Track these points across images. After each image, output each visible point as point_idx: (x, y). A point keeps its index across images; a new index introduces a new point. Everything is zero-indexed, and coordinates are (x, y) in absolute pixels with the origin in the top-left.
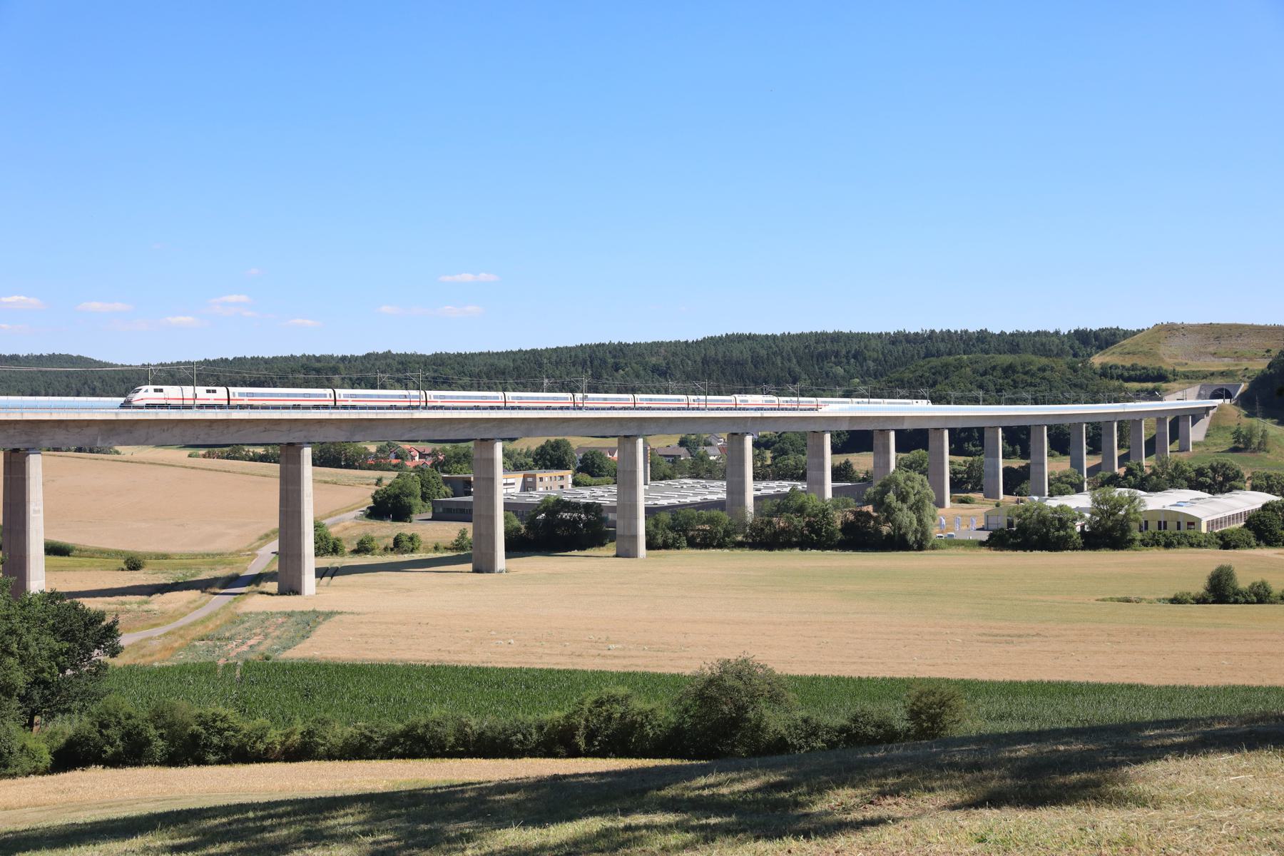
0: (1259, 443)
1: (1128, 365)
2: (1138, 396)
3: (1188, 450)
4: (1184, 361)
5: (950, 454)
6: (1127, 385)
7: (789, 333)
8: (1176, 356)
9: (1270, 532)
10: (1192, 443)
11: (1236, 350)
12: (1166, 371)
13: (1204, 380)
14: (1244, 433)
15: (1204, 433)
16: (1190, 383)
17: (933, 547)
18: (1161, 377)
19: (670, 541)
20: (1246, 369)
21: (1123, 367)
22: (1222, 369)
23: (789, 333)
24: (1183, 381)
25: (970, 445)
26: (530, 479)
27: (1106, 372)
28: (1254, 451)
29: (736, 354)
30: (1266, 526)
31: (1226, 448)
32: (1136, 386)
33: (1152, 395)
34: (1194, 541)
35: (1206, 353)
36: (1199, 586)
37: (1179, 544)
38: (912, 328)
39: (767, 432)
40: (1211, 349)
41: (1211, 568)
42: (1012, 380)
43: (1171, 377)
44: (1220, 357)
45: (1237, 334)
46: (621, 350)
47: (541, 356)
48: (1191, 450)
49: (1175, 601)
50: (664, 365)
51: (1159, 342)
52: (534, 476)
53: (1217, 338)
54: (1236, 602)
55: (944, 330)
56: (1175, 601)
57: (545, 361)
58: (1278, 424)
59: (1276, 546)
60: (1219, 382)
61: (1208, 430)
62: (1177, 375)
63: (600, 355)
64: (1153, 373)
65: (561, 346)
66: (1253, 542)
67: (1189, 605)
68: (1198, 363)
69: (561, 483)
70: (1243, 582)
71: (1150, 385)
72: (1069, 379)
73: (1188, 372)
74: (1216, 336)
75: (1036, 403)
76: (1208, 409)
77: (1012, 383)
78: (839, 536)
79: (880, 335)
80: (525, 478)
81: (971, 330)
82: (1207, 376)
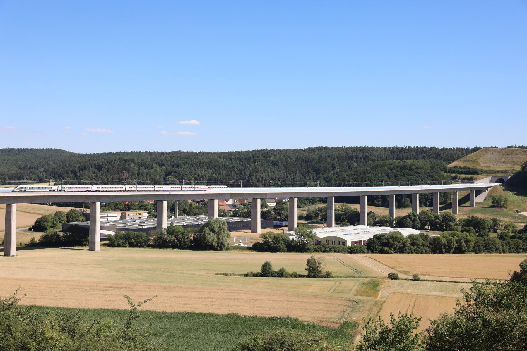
0: (504, 204)
1: (462, 166)
2: (464, 180)
3: (473, 206)
4: (489, 165)
5: (367, 205)
6: (459, 175)
7: (345, 147)
8: (486, 163)
9: (373, 247)
10: (476, 203)
11: (513, 161)
12: (478, 170)
13: (494, 174)
14: (497, 199)
15: (484, 198)
16: (487, 175)
17: (227, 249)
18: (475, 172)
19: (121, 244)
20: (513, 170)
21: (460, 167)
22: (502, 169)
23: (345, 147)
24: (485, 174)
25: (377, 201)
26: (124, 215)
27: (455, 170)
28: (501, 207)
29: (311, 156)
30: (372, 244)
31: (490, 205)
32: (463, 176)
33: (471, 181)
34: (337, 250)
35: (500, 162)
36: (259, 270)
37: (330, 251)
38: (401, 145)
39: (108, 201)
40: (503, 160)
41: (263, 262)
42: (402, 173)
43: (479, 172)
44: (506, 164)
45: (516, 154)
46: (268, 153)
47: (232, 155)
48: (475, 206)
49: (247, 275)
50: (276, 161)
51: (480, 156)
52: (125, 213)
53: (507, 155)
54: (268, 276)
55: (415, 147)
56: (247, 275)
57: (233, 157)
58: (516, 194)
59: (375, 253)
60: (500, 175)
61: (486, 197)
62: (483, 172)
63: (257, 155)
64: (472, 170)
65: (318, 146)
66: (366, 250)
67: (250, 277)
68: (496, 166)
69: (140, 216)
70: (325, 268)
71: (469, 176)
72: (428, 173)
73: (488, 170)
74: (507, 154)
75: (321, 187)
76: (487, 188)
77: (402, 174)
78: (189, 243)
79: (385, 149)
80: (122, 214)
81: (427, 147)
82: (496, 172)
